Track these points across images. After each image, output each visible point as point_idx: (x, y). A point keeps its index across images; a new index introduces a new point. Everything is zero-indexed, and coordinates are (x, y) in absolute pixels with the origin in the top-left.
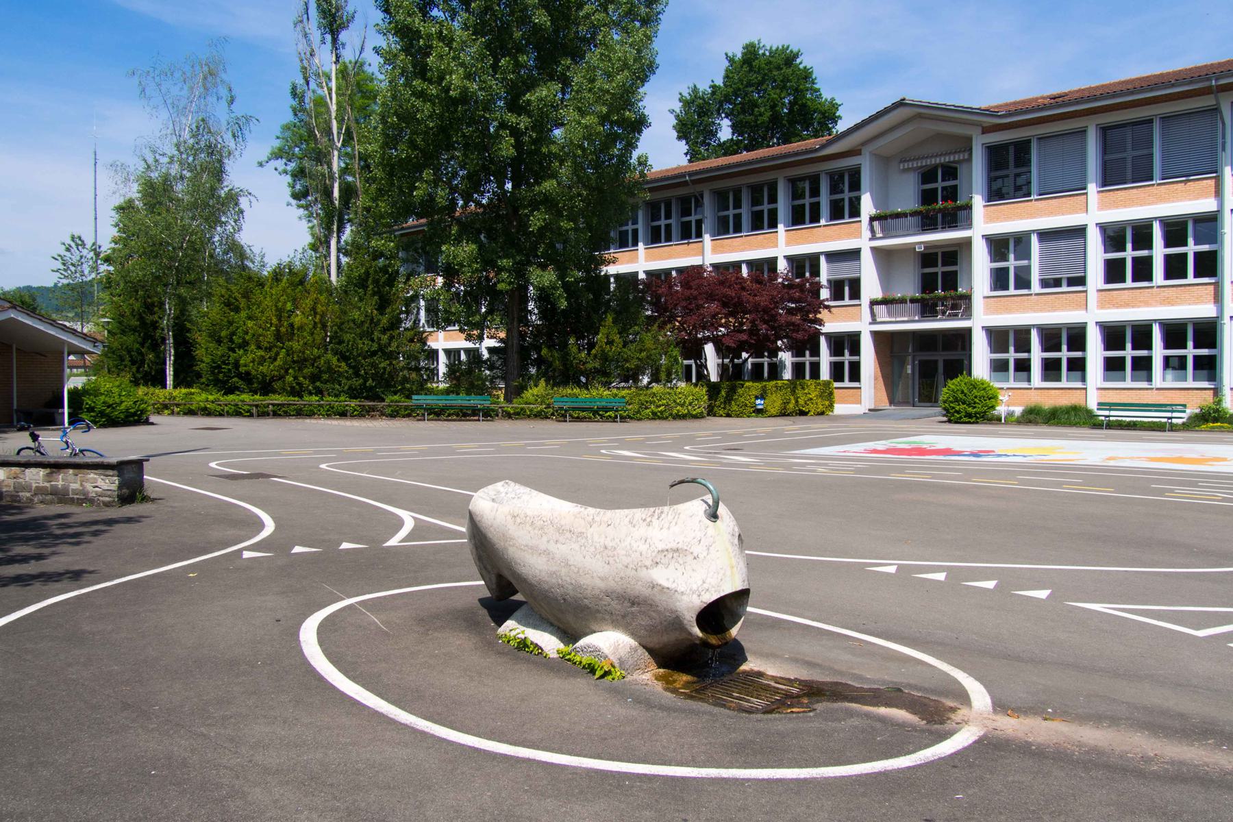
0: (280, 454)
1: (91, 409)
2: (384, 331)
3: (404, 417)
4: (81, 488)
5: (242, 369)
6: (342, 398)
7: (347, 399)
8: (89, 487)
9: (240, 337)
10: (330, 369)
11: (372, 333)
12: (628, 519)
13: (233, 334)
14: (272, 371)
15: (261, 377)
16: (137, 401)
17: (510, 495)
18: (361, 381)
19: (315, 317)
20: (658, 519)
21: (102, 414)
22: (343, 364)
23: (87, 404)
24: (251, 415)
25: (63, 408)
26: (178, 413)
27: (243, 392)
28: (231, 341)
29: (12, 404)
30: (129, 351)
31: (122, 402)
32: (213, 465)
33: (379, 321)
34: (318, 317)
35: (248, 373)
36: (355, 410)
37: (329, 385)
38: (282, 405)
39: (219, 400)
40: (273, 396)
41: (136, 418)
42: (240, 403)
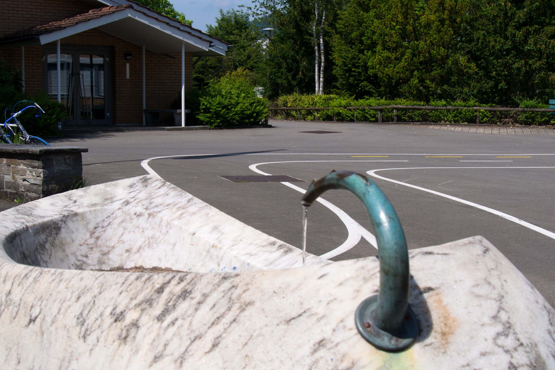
0: (349, 158)
1: (207, 110)
2: (518, 27)
3: (540, 124)
4: (13, 181)
5: (371, 72)
6: (472, 102)
7: (477, 104)
8: (19, 179)
9: (369, 38)
10: (461, 73)
11: (506, 30)
12: (76, 309)
13: (362, 35)
14: (397, 73)
15: (386, 80)
16: (254, 103)
17: (132, 209)
18: (491, 83)
19: (443, 13)
20: (160, 318)
21: (217, 115)
22: (473, 65)
23: (204, 104)
24: (376, 121)
25: (181, 108)
26: (319, 119)
27: (370, 94)
28: (361, 42)
29: (142, 104)
30: (284, 58)
31: (238, 104)
32: (253, 168)
33: (514, 14)
34: (446, 12)
35: (375, 76)
36: (485, 116)
37: (457, 89)
38: (406, 110)
39: (349, 105)
40: (399, 100)
41: (252, 120)
42: (367, 108)
